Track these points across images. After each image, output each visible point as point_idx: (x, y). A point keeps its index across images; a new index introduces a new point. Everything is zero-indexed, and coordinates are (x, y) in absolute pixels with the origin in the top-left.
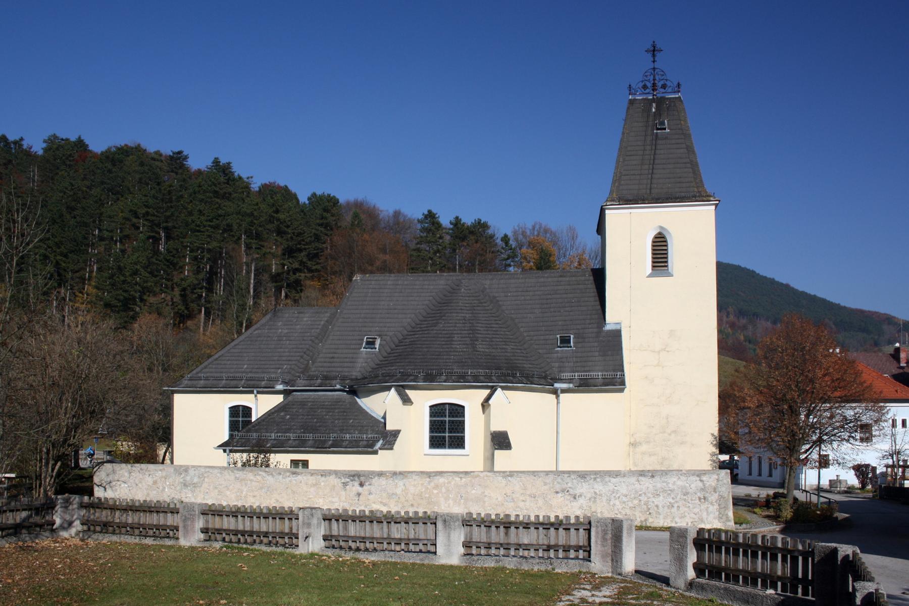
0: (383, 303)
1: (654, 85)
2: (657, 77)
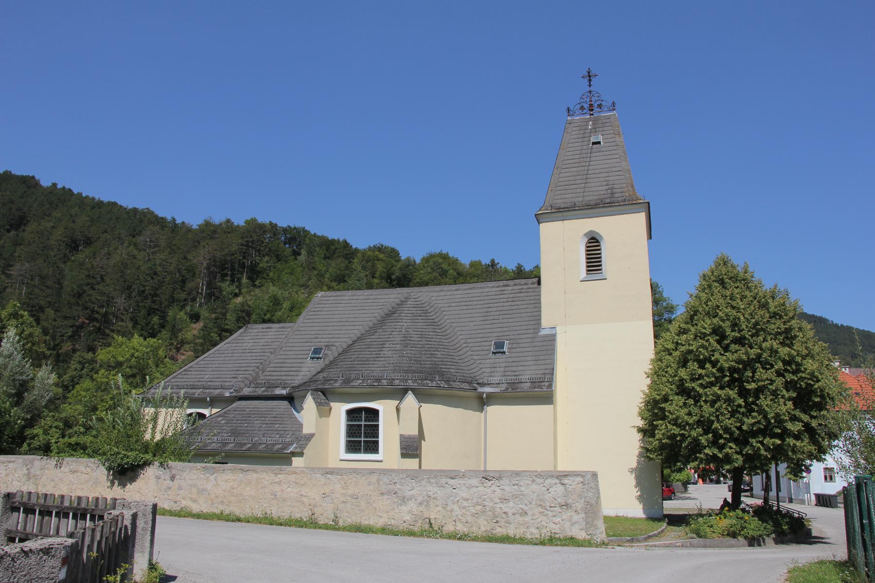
0: (338, 315)
1: (591, 105)
2: (593, 99)
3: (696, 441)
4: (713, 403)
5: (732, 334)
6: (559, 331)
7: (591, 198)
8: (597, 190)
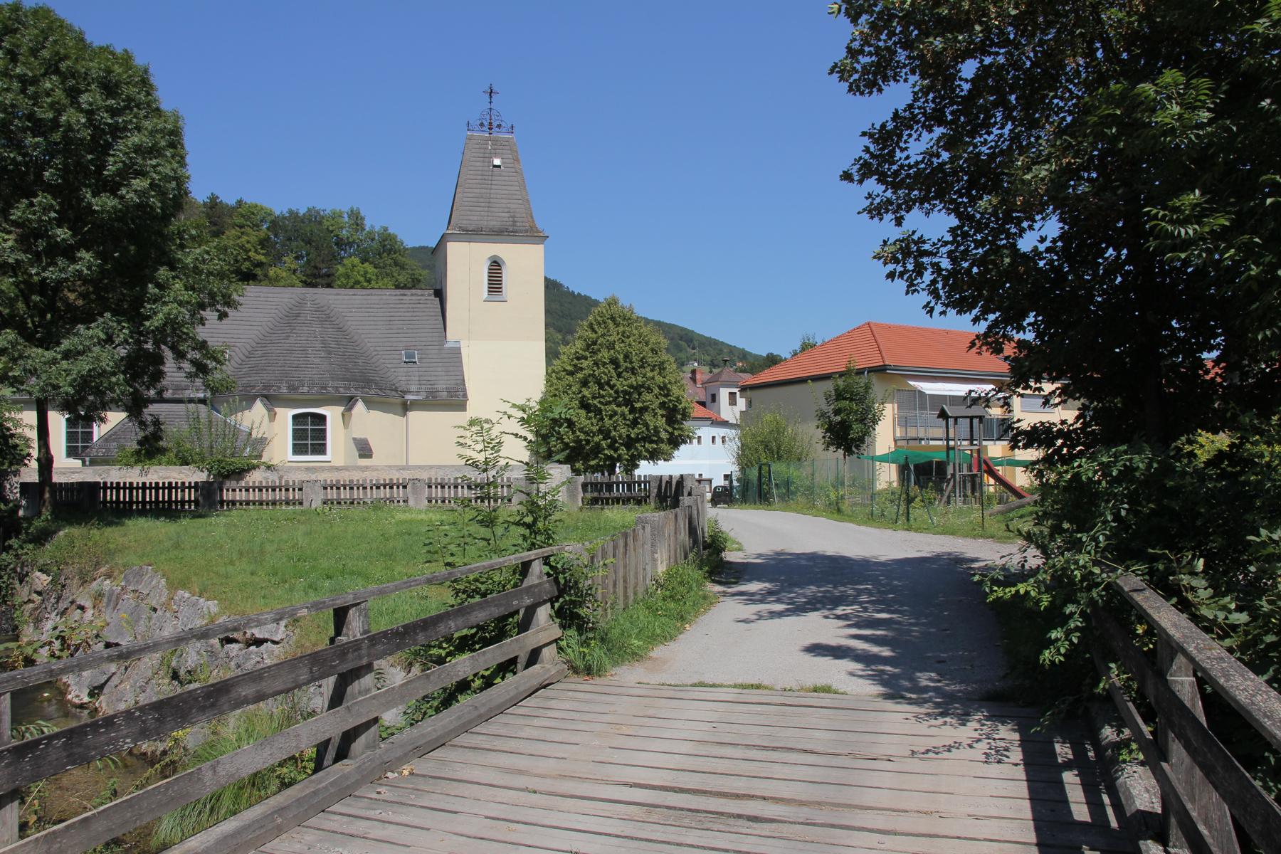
3: (598, 445)
4: (611, 417)
5: (624, 365)
6: (463, 345)
7: (494, 224)
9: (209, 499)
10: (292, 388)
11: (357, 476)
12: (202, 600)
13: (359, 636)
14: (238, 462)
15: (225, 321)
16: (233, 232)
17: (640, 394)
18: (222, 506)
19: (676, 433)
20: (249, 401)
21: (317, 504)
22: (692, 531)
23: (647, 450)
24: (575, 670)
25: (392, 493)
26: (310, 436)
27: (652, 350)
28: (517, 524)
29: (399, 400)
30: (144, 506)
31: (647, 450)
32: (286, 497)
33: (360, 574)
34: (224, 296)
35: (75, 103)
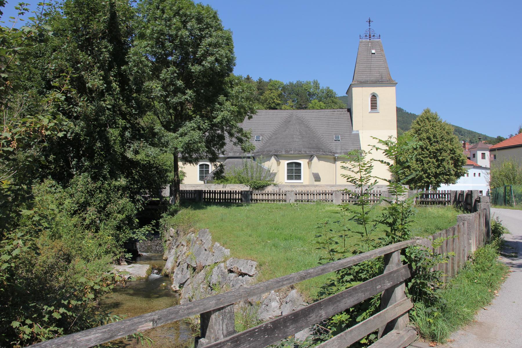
3: (421, 176)
4: (427, 163)
5: (433, 140)
7: (373, 79)
8: (375, 76)
9: (246, 198)
10: (287, 152)
11: (312, 189)
12: (224, 248)
13: (222, 339)
14: (262, 183)
15: (251, 120)
16: (268, 92)
17: (441, 153)
18: (252, 201)
19: (459, 171)
20: (268, 157)
21: (292, 201)
22: (487, 224)
23: (445, 179)
24: (423, 336)
25: (326, 197)
26: (294, 172)
27: (447, 132)
28: (382, 222)
29: (332, 157)
30: (220, 200)
31: (445, 179)
32: (280, 198)
33: (300, 239)
34: (250, 109)
35: (185, 26)
